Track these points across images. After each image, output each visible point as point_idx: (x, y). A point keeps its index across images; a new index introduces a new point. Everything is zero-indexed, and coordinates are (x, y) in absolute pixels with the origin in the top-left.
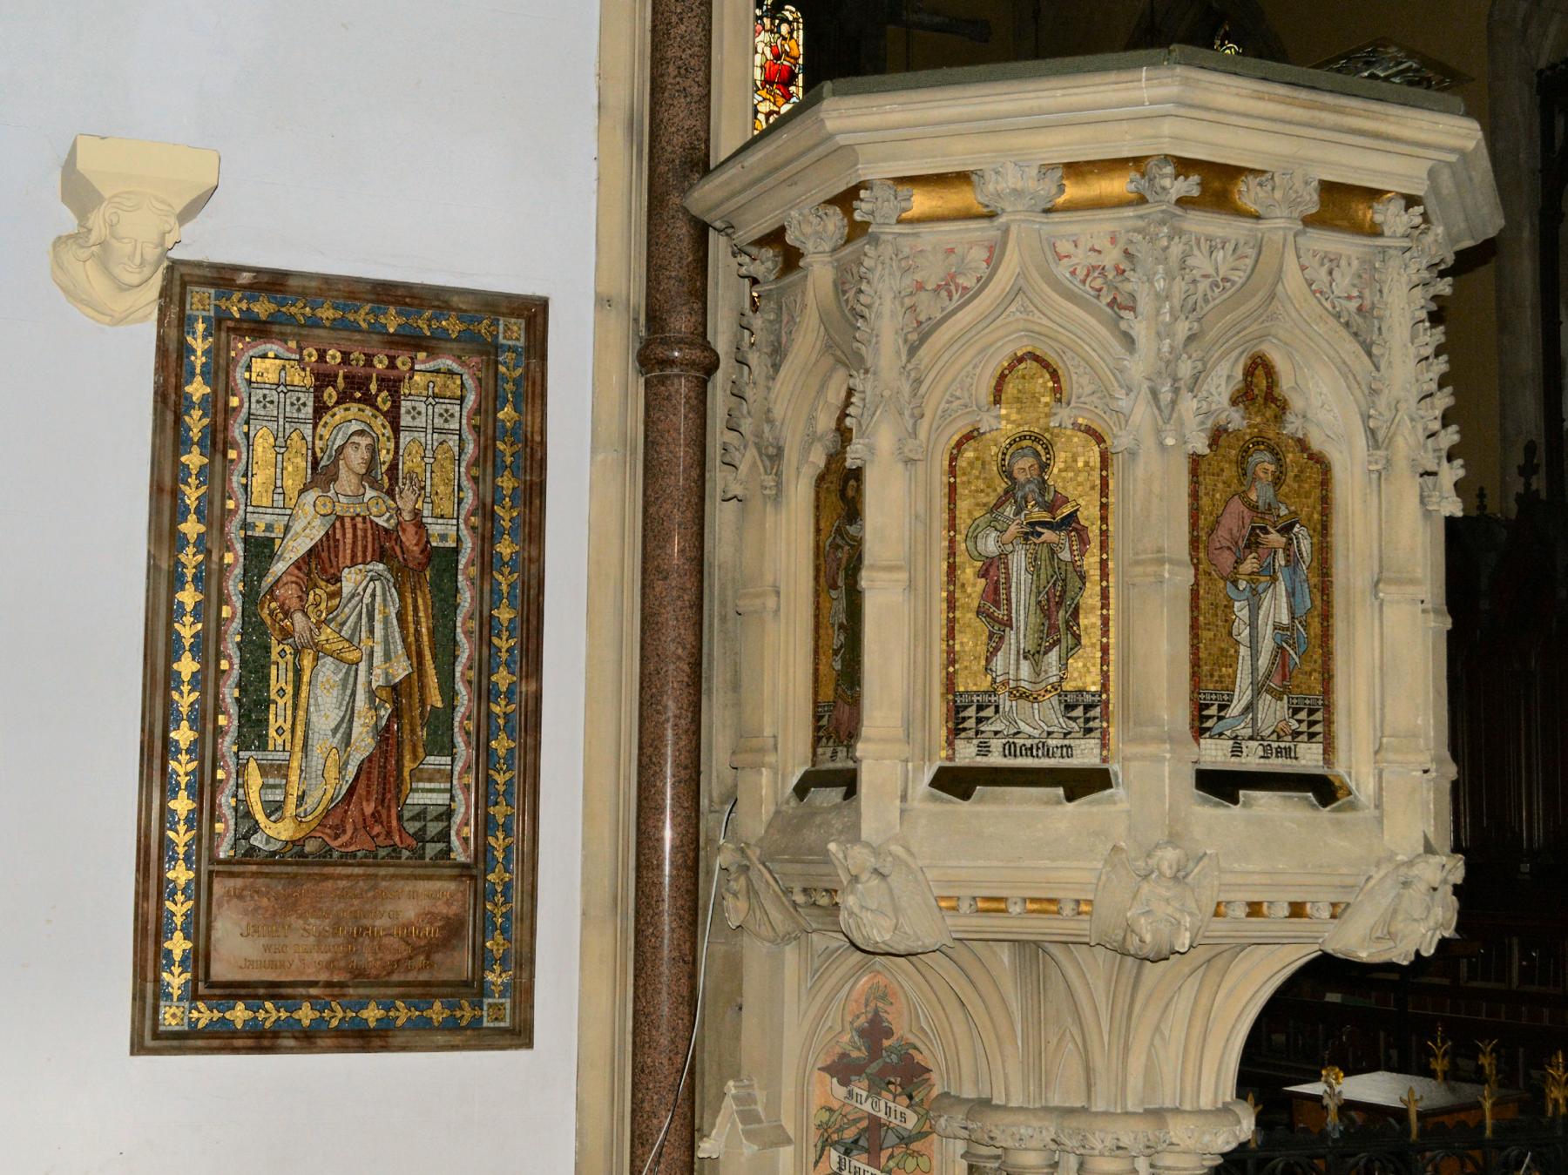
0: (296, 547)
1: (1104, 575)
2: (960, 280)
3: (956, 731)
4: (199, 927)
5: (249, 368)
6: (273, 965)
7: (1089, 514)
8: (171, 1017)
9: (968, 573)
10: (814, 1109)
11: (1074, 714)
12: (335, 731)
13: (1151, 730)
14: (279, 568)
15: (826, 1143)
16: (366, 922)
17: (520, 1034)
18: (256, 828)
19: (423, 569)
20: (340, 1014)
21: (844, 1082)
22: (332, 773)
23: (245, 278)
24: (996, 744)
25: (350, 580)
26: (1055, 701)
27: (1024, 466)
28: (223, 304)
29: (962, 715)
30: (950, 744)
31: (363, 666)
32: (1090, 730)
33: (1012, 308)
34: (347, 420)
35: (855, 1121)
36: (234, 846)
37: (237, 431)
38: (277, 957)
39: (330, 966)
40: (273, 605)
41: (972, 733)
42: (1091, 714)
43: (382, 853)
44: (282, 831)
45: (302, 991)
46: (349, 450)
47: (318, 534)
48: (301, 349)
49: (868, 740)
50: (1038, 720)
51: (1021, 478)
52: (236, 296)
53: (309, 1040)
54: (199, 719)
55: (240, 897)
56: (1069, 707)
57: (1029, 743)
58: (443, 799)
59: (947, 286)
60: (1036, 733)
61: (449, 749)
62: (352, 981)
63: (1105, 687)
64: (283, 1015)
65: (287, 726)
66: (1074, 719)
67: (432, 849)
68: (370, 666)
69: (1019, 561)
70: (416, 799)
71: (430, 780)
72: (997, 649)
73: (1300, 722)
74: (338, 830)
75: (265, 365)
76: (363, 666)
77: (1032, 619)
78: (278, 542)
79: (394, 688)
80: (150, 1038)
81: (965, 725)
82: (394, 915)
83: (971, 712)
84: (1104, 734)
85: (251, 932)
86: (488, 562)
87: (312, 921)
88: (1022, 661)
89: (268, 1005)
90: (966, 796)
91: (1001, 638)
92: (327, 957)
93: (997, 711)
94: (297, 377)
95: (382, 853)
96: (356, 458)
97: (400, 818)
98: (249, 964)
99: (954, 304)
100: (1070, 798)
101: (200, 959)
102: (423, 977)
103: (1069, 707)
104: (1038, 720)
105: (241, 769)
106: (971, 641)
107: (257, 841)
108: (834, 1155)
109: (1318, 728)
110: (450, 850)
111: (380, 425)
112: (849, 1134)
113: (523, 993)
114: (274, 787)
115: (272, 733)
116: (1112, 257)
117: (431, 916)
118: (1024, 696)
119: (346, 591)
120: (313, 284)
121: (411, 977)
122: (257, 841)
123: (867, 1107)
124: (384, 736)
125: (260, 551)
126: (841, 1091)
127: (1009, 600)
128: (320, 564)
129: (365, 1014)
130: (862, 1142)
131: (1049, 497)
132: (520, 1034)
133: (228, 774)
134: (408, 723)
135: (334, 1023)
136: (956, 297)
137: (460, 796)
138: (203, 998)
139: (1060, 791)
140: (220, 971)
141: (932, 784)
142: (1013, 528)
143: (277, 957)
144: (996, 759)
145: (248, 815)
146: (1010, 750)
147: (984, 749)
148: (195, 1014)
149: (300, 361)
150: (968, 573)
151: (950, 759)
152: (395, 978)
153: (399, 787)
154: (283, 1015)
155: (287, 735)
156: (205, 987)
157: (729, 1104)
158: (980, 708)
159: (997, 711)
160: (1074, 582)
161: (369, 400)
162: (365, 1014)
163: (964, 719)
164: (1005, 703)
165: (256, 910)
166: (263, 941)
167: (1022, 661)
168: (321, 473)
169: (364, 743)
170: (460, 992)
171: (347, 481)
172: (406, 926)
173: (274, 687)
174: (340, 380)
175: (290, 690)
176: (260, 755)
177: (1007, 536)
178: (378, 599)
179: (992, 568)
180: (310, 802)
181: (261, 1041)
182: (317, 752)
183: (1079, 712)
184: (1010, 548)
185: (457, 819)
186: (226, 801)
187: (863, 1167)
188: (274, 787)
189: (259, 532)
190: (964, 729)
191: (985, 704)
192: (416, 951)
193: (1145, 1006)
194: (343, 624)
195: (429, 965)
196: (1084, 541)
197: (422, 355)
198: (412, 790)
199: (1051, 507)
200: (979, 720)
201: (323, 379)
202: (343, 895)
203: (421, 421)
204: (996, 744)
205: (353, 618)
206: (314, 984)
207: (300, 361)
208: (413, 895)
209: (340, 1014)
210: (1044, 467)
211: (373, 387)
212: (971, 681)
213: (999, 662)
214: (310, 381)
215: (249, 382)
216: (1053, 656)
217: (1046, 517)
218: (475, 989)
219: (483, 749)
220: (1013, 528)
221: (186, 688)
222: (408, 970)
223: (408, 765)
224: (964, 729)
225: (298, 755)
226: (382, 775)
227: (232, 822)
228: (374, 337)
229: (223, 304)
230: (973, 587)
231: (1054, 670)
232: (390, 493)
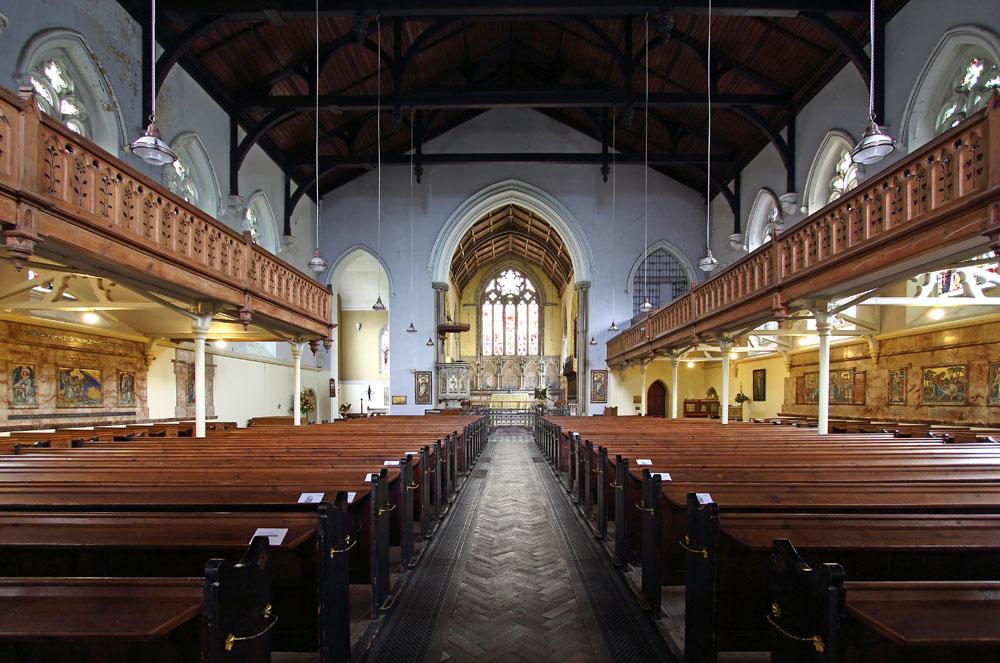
134: (426, 390)
228: (424, 373)
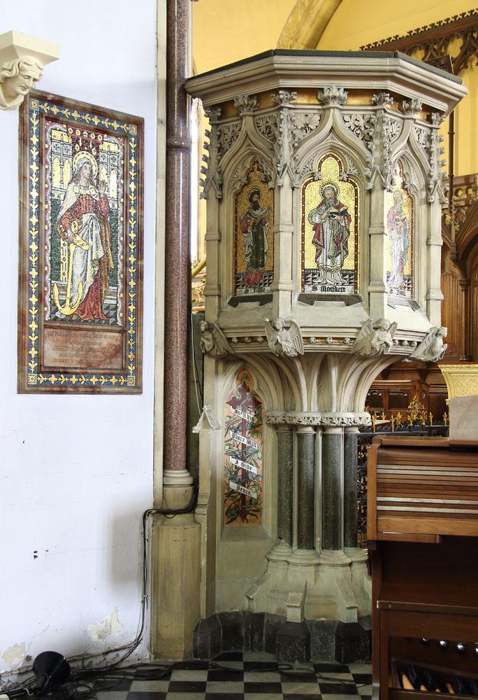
0: (67, 205)
1: (356, 231)
2: (310, 126)
3: (304, 283)
4: (39, 346)
5: (51, 133)
6: (63, 361)
7: (351, 212)
8: (32, 379)
9: (309, 227)
10: (225, 416)
11: (345, 277)
12: (81, 275)
13: (378, 282)
14: (61, 213)
15: (229, 429)
16: (91, 346)
17: (137, 389)
18: (57, 310)
19: (104, 216)
20: (84, 380)
21: (234, 408)
22: (81, 291)
23: (50, 97)
24: (319, 287)
25: (86, 218)
26: (339, 273)
27: (329, 193)
28: (42, 106)
29: (307, 276)
30: (303, 286)
31: (89, 252)
32: (351, 283)
33: (328, 138)
34: (83, 156)
35: (238, 421)
36: (50, 317)
37: (48, 157)
38: (64, 358)
39: (80, 362)
40: (61, 226)
41: (311, 283)
42: (351, 277)
43: (97, 321)
44: (66, 311)
45: (74, 370)
46: (84, 168)
47: (75, 200)
48: (68, 128)
49: (281, 283)
50: (334, 279)
51: (328, 197)
52: (46, 104)
53: (76, 390)
54: (39, 268)
55: (52, 335)
56: (344, 275)
57: (330, 287)
58: (114, 302)
59: (306, 127)
60: (333, 283)
61: (115, 284)
62: (87, 368)
63: (356, 269)
64: (67, 379)
65: (66, 272)
66: (346, 279)
67: (112, 320)
68: (92, 252)
69: (326, 226)
70: (106, 302)
71: (111, 295)
72: (319, 254)
73: (346, 279)
74: (83, 312)
75: (58, 134)
76: (89, 252)
77: (331, 245)
78: (62, 202)
79: (100, 261)
80: (21, 390)
81: (309, 280)
82: (100, 344)
83: (310, 276)
84: (356, 283)
85: (56, 348)
86: (126, 215)
87: (75, 345)
88: (328, 260)
89: (62, 376)
90: (312, 304)
91: (321, 251)
92: (79, 359)
93: (319, 276)
94: (66, 139)
95: (97, 321)
96: (86, 172)
97: (101, 307)
98: (55, 360)
99: (307, 135)
100: (348, 305)
101: (39, 358)
102: (109, 367)
103: (344, 275)
104: (334, 279)
105: (52, 287)
106: (311, 250)
107: (57, 314)
108: (231, 433)
109: (410, 286)
110: (117, 321)
111: (93, 160)
112: (236, 425)
113: (138, 373)
114: (63, 295)
115: (62, 274)
116: (362, 123)
117: (111, 345)
118: (330, 271)
119: (84, 223)
120: (73, 103)
121: (105, 367)
122: (57, 314)
123: (242, 416)
124: (97, 278)
125: (56, 206)
126: (233, 411)
127: (323, 238)
128: (75, 212)
129: (91, 380)
130: (240, 428)
131: (337, 204)
132: (137, 389)
133: (48, 289)
134: (103, 274)
135: (82, 383)
136: (308, 132)
137: (120, 302)
138: (42, 373)
139: (343, 302)
140: (48, 363)
141: (299, 300)
142: (325, 214)
143: (64, 358)
144: (319, 292)
145: (55, 304)
146: (324, 289)
147: (315, 288)
148: (39, 379)
149: (67, 132)
150: (309, 227)
151: (304, 291)
152: (101, 367)
153: (101, 297)
154: (67, 379)
155: (66, 275)
156: (41, 370)
157: (201, 420)
158: (314, 274)
159: (319, 276)
160: (346, 233)
161: (89, 151)
162: (91, 380)
163: (308, 278)
164: (322, 272)
165: (57, 340)
166: (60, 352)
167: (328, 260)
168: (75, 178)
169: (90, 281)
170: (117, 373)
171: (83, 182)
172: (104, 348)
173: (62, 257)
174: (80, 141)
175: (67, 259)
176: (57, 282)
177: (323, 217)
178: (94, 226)
179: (317, 228)
180: (74, 301)
181: (61, 390)
182: (76, 283)
183: (347, 277)
184: (324, 221)
185: (119, 310)
186: (48, 299)
187: (241, 436)
188: (63, 295)
189: (56, 197)
190: (308, 282)
191: (314, 273)
192: (107, 357)
193: (460, 336)
194: (83, 235)
195: (111, 363)
196: (350, 220)
197: (105, 136)
198: (105, 299)
199: (338, 207)
200: (313, 279)
201: (75, 141)
202: (85, 336)
203: (106, 161)
204: (319, 287)
205: (86, 233)
206: (77, 368)
207: (67, 132)
208: (106, 337)
209: (64, 380)
210: (336, 194)
211: (91, 146)
212: (310, 264)
213: (320, 260)
214: (70, 141)
215: (51, 139)
216: (339, 257)
217: (336, 211)
218: (124, 372)
219: (126, 284)
220: (325, 214)
221: (34, 256)
222: (105, 364)
223: (104, 289)
224: (308, 282)
225: (70, 284)
226: (95, 294)
227: (49, 307)
229: (42, 106)
230: (310, 234)
231: (339, 263)
232: (97, 188)
